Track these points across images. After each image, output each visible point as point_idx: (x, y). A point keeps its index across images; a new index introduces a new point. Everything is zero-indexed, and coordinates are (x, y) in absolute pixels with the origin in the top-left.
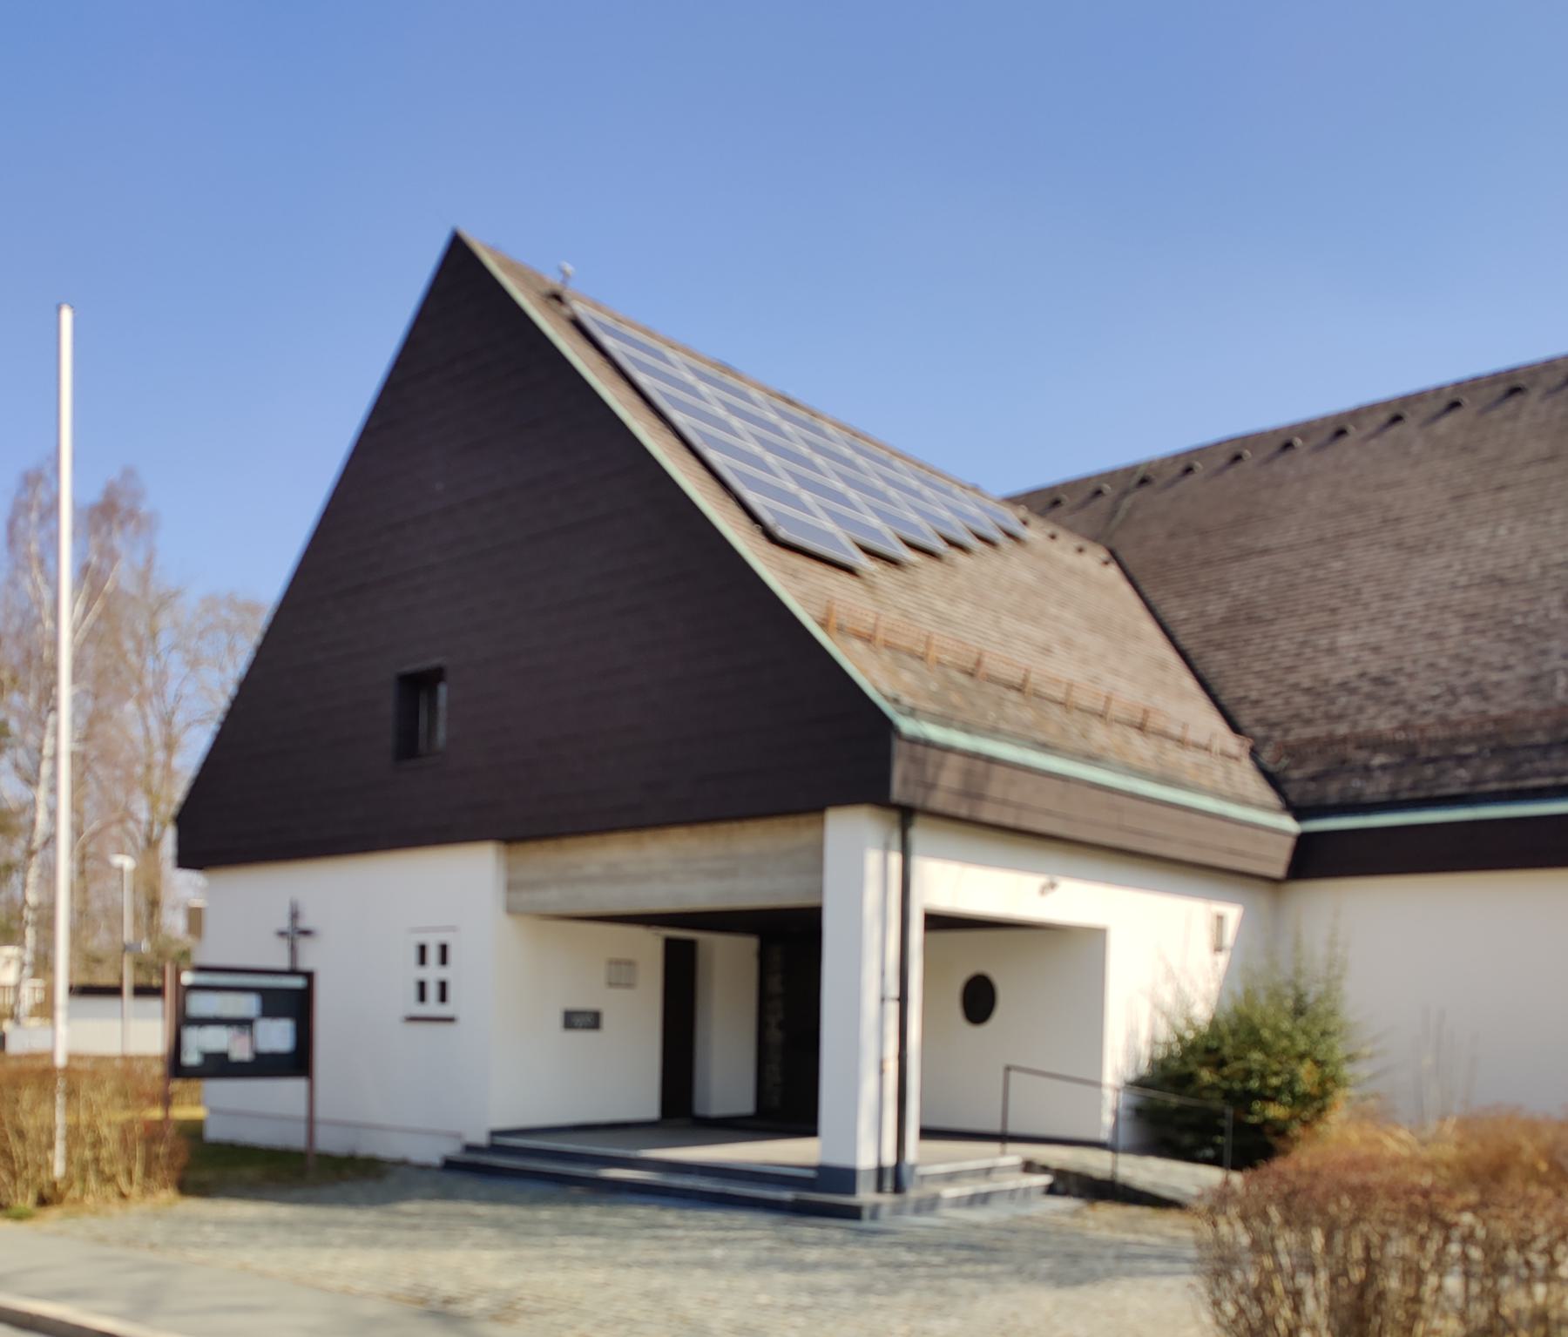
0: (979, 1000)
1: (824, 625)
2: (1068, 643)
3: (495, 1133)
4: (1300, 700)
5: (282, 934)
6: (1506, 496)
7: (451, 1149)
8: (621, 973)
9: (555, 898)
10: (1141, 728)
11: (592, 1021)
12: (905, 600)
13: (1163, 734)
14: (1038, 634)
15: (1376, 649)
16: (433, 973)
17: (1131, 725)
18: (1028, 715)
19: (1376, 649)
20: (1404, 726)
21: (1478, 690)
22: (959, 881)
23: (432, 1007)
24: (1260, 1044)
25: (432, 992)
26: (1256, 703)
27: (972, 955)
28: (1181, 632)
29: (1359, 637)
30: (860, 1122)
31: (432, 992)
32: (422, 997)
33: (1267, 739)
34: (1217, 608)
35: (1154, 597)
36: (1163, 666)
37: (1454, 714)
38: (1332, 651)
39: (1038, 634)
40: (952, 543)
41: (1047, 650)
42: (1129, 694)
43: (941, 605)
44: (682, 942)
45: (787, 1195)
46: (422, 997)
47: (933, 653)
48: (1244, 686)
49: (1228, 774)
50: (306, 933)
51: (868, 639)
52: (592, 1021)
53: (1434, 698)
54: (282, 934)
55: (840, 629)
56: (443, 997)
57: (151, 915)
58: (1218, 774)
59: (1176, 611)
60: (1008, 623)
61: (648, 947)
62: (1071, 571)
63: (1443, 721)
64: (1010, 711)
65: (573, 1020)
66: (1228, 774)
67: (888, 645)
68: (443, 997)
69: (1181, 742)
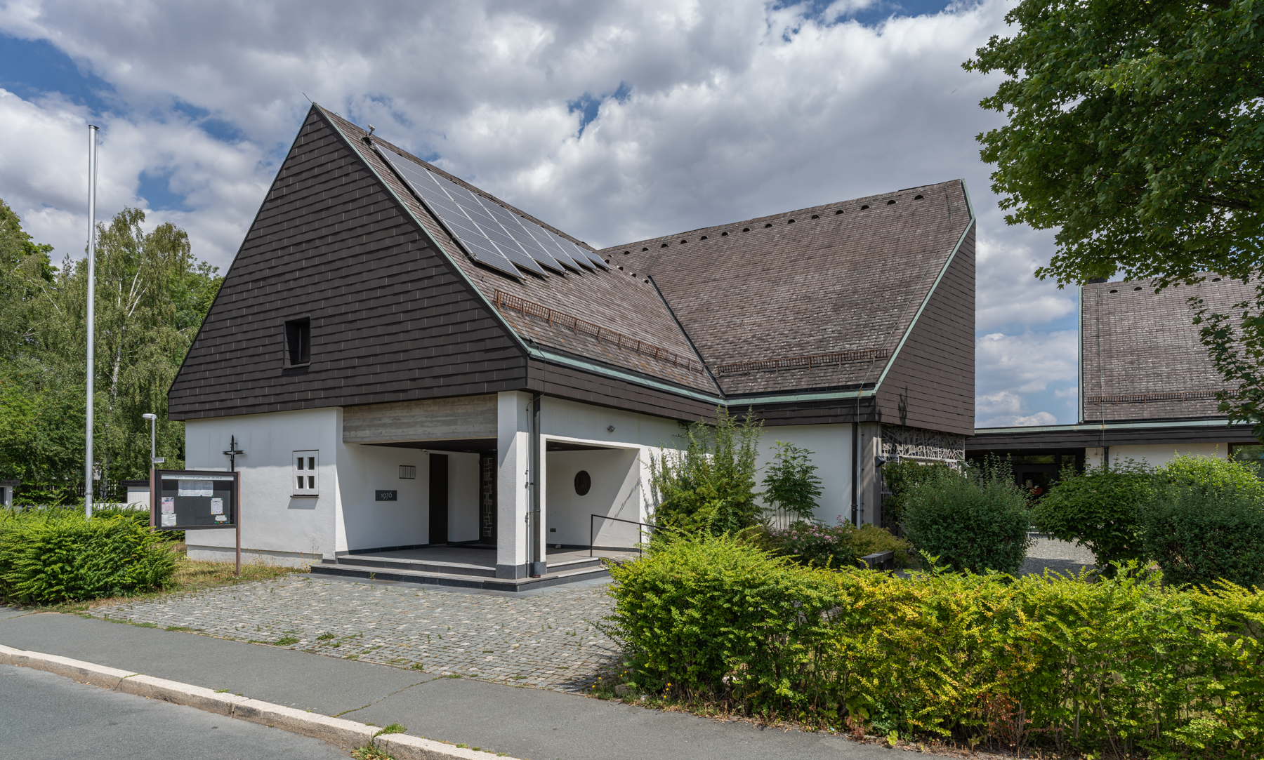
0: (583, 483)
1: (495, 303)
2: (623, 317)
3: (337, 553)
4: (728, 346)
5: (226, 453)
6: (811, 261)
7: (317, 563)
8: (407, 472)
9: (367, 435)
10: (655, 357)
11: (393, 496)
12: (542, 293)
13: (667, 360)
14: (608, 312)
15: (759, 325)
16: (306, 472)
17: (651, 355)
18: (598, 349)
19: (759, 325)
20: (770, 360)
21: (799, 345)
22: (566, 428)
23: (307, 490)
24: (1178, 470)
25: (306, 482)
26: (710, 347)
27: (577, 463)
28: (679, 314)
29: (752, 320)
30: (515, 548)
31: (306, 482)
32: (301, 486)
33: (715, 363)
34: (694, 304)
35: (668, 298)
36: (670, 329)
37: (790, 354)
38: (741, 325)
39: (608, 312)
40: (590, 270)
41: (613, 320)
42: (650, 340)
43: (560, 296)
44: (439, 458)
45: (482, 579)
46: (301, 486)
47: (552, 318)
48: (704, 340)
49: (696, 379)
50: (240, 452)
51: (520, 311)
52: (393, 496)
53: (782, 348)
54: (226, 453)
55: (503, 305)
56: (312, 486)
57: (535, 415)
58: (691, 379)
59: (676, 304)
60: (594, 306)
61: (422, 459)
62: (629, 284)
63: (786, 357)
64: (590, 347)
65: (380, 496)
66: (696, 379)
67: (528, 314)
68: (312, 486)
69: (675, 364)
